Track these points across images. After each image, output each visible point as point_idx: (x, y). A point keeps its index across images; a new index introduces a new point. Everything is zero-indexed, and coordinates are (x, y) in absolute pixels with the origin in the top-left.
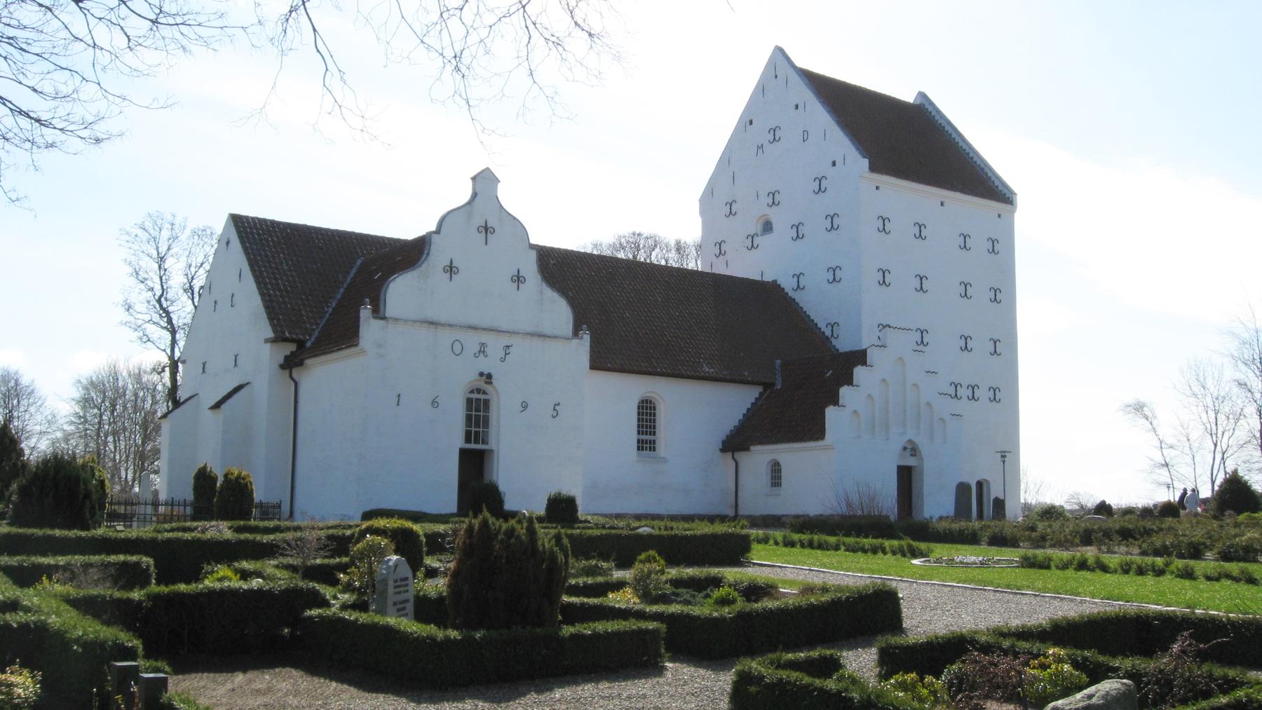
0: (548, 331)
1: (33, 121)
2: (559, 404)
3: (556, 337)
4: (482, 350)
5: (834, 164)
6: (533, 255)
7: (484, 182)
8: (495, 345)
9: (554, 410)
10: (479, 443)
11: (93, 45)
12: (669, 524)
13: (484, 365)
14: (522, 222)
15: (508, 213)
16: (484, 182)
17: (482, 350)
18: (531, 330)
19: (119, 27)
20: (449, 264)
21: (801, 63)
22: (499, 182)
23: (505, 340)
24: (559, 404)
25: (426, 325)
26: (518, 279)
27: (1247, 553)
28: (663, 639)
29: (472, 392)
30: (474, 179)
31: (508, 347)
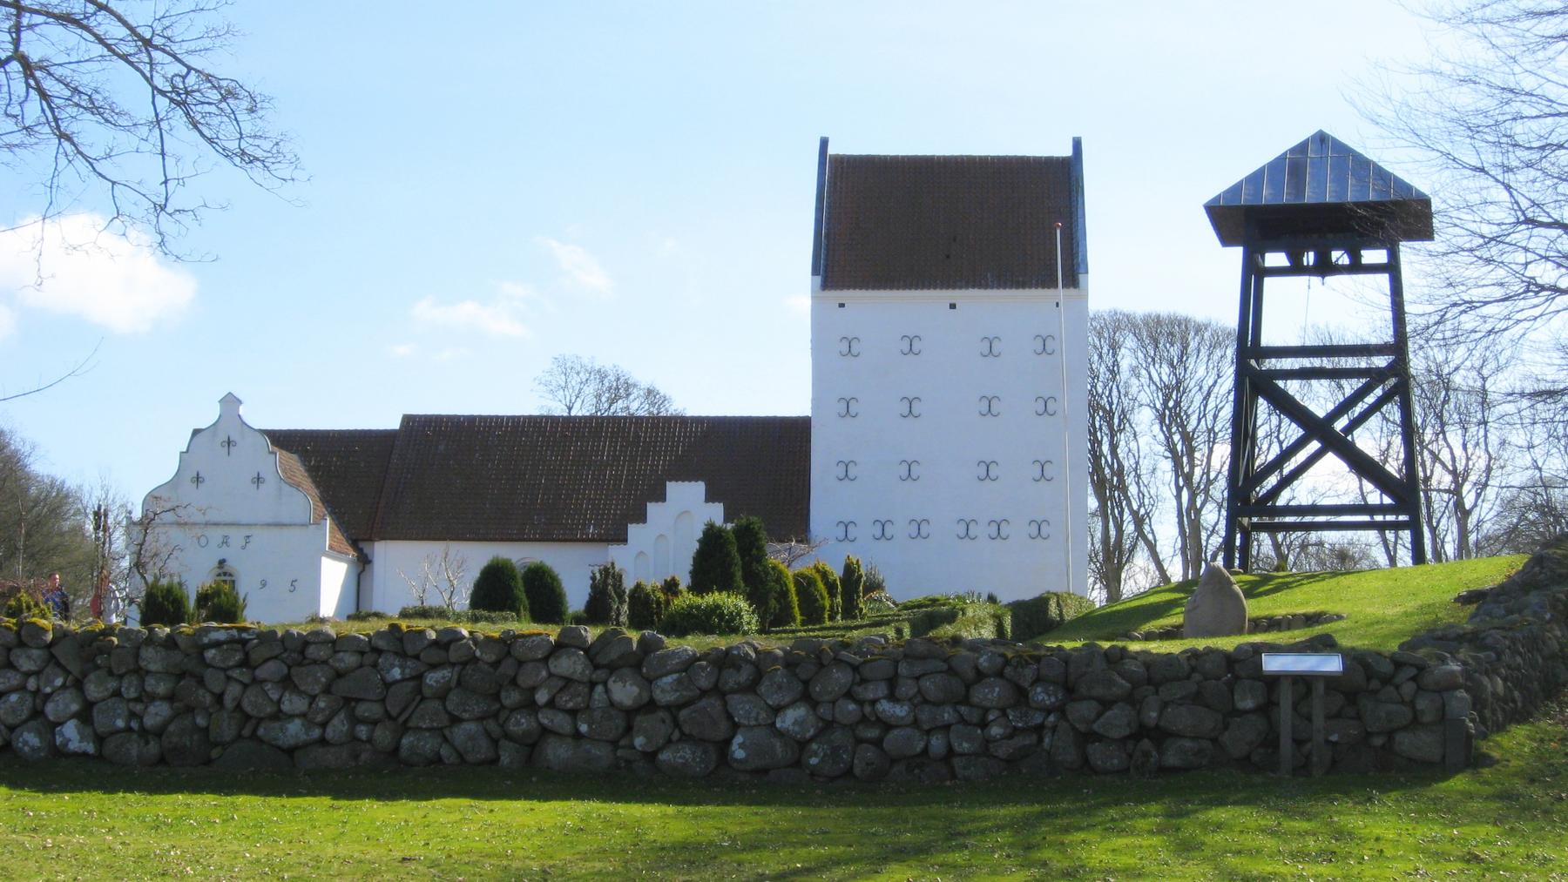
0: (286, 520)
1: (82, 59)
2: (296, 581)
3: (295, 525)
4: (225, 541)
5: (842, 305)
6: (273, 463)
7: (230, 402)
8: (237, 536)
9: (292, 585)
10: (1056, 286)
11: (157, 17)
12: (1211, 366)
13: (224, 553)
14: (156, 486)
15: (180, 462)
16: (230, 402)
17: (225, 541)
18: (270, 521)
19: (151, 29)
20: (256, 476)
21: (256, 428)
22: (240, 402)
23: (245, 532)
24: (296, 581)
25: (175, 526)
26: (258, 480)
27: (3, 869)
28: (1281, 472)
29: (219, 575)
30: (220, 402)
31: (248, 537)
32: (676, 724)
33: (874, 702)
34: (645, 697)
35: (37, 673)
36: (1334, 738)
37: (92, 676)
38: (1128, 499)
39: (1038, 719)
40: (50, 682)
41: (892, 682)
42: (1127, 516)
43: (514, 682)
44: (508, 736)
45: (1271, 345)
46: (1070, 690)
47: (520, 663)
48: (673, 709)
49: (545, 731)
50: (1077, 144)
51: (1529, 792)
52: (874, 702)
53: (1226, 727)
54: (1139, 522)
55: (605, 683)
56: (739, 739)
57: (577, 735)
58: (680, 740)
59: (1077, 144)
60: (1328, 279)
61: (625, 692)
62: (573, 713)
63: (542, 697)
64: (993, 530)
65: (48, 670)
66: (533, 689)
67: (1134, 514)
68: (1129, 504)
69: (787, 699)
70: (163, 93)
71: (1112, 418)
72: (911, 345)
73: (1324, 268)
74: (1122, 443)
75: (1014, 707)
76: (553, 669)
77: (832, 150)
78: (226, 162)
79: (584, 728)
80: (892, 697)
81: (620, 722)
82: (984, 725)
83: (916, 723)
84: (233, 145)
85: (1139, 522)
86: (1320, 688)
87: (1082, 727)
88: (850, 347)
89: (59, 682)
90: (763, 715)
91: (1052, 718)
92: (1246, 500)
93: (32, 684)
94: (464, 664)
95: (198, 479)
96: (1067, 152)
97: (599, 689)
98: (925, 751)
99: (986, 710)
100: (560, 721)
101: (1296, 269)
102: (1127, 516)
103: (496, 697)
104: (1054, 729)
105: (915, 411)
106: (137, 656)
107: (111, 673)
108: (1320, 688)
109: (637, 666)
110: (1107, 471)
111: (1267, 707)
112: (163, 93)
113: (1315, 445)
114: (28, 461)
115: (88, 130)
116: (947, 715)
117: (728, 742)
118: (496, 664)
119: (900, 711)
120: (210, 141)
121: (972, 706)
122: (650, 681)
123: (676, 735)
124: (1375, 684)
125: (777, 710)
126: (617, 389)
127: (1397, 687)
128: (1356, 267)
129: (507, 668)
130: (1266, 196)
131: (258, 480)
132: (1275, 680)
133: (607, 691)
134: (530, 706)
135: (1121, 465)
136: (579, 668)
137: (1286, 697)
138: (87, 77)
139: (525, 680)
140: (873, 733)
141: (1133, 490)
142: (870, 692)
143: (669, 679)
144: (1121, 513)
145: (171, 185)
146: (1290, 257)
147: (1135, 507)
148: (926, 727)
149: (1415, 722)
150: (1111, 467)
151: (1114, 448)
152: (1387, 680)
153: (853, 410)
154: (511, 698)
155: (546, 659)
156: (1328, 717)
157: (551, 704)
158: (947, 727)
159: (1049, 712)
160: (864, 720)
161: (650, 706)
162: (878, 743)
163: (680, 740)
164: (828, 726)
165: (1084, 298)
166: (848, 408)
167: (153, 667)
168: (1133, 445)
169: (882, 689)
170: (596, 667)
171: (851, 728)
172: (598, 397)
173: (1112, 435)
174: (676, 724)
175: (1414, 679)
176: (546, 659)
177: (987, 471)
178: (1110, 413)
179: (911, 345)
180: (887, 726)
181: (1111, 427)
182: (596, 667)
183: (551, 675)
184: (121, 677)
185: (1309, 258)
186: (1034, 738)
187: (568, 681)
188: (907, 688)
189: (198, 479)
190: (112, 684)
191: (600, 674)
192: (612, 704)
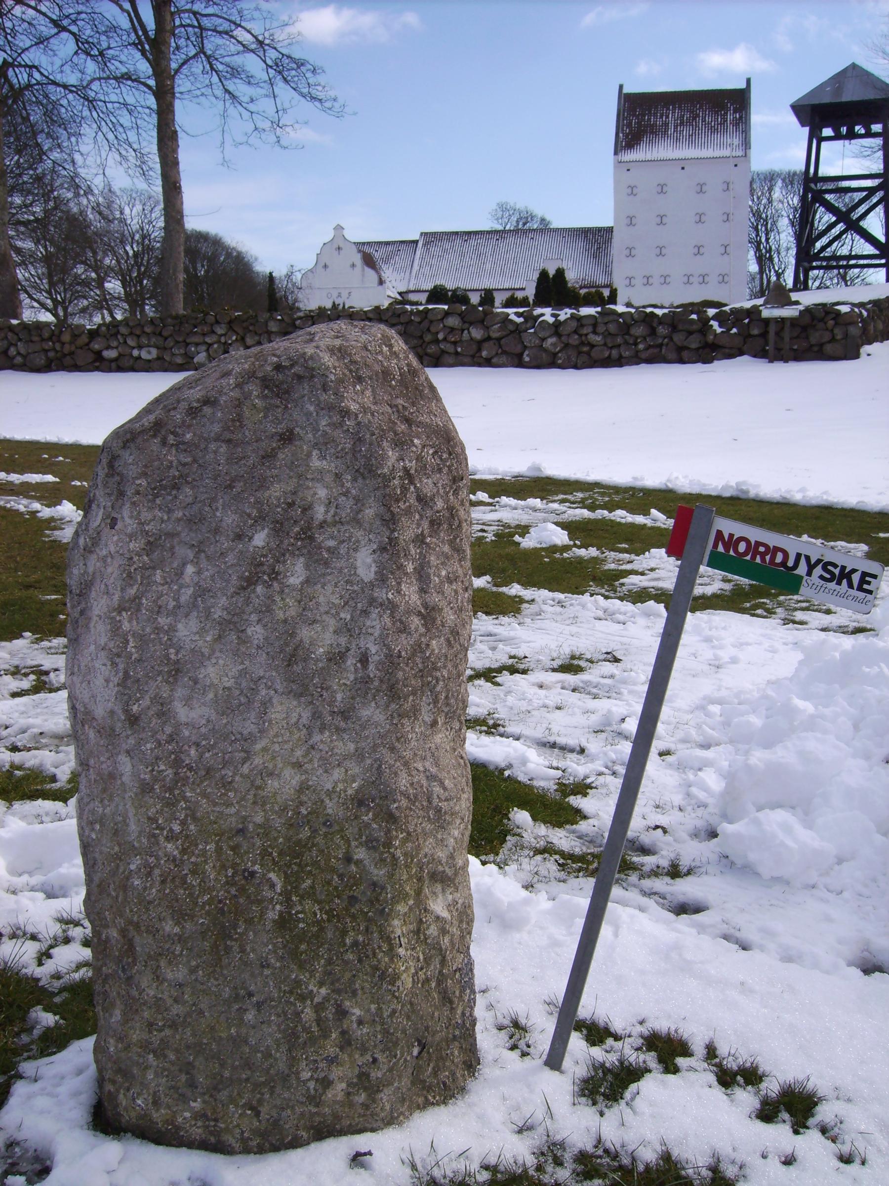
7: (339, 228)
16: (339, 228)
26: (353, 266)
32: (500, 346)
33: (586, 335)
34: (486, 336)
35: (224, 335)
36: (795, 347)
37: (248, 335)
38: (773, 265)
39: (660, 341)
40: (230, 338)
41: (595, 325)
42: (772, 272)
43: (428, 330)
44: (427, 354)
45: (825, 175)
46: (674, 328)
47: (431, 322)
48: (499, 340)
49: (443, 352)
50: (748, 81)
51: (104, 45)
52: (586, 335)
53: (745, 343)
54: (778, 275)
55: (468, 330)
56: (527, 352)
57: (457, 353)
58: (501, 353)
59: (748, 81)
60: (852, 141)
61: (477, 333)
62: (455, 343)
63: (441, 336)
64: (701, 279)
65: (229, 333)
66: (437, 333)
67: (776, 272)
68: (774, 267)
69: (548, 334)
70: (271, 67)
71: (767, 223)
72: (662, 189)
73: (852, 136)
74: (772, 237)
75: (649, 336)
76: (446, 324)
77: (626, 90)
78: (303, 100)
79: (459, 350)
80: (595, 332)
81: (475, 347)
82: (636, 344)
83: (605, 344)
84: (305, 91)
85: (778, 275)
86: (788, 324)
87: (679, 344)
88: (632, 190)
89: (234, 338)
90: (537, 341)
91: (666, 340)
92: (807, 253)
93: (223, 340)
94: (407, 323)
95: (325, 266)
96: (743, 85)
97: (466, 332)
98: (610, 356)
99: (637, 338)
100: (450, 348)
101: (838, 137)
102: (772, 272)
103: (421, 337)
104: (667, 345)
105: (664, 222)
106: (267, 326)
107: (256, 333)
108: (788, 324)
109: (482, 321)
110: (764, 251)
111: (764, 335)
112: (271, 67)
113: (840, 227)
114: (254, 265)
115: (238, 87)
116: (619, 340)
117: (522, 354)
118: (420, 323)
119: (598, 339)
120: (294, 89)
121: (631, 335)
122: (487, 328)
123: (500, 351)
124: (815, 322)
125: (543, 340)
126: (527, 218)
127: (825, 323)
128: (869, 134)
129: (425, 324)
130: (826, 100)
131: (353, 266)
132: (767, 321)
133: (469, 332)
134: (437, 341)
135: (770, 248)
136: (457, 323)
137: (772, 329)
138: (238, 60)
139: (433, 329)
140: (585, 349)
141: (776, 260)
142: (585, 331)
143: (496, 327)
144: (770, 271)
145: (280, 113)
146: (834, 131)
147: (777, 269)
148: (610, 345)
149: (833, 340)
150: (766, 248)
151: (767, 240)
152: (821, 320)
153: (633, 222)
154: (428, 338)
155: (442, 319)
156: (791, 339)
157: (445, 339)
158: (619, 346)
159: (665, 338)
160: (582, 343)
161: (489, 338)
162: (588, 353)
163: (501, 353)
164: (567, 346)
165: (749, 162)
166: (631, 221)
167: (274, 330)
168: (777, 238)
169: (590, 329)
170: (464, 322)
171: (577, 347)
172: (518, 222)
173: (767, 234)
174: (500, 346)
175: (833, 319)
176: (442, 319)
177: (699, 250)
178: (766, 220)
179: (662, 189)
180: (592, 346)
181: (766, 229)
182: (464, 322)
183: (444, 326)
184: (260, 335)
185: (844, 130)
186: (658, 349)
187: (452, 329)
188: (601, 329)
189: (325, 266)
190: (257, 338)
191: (467, 325)
192: (472, 339)
